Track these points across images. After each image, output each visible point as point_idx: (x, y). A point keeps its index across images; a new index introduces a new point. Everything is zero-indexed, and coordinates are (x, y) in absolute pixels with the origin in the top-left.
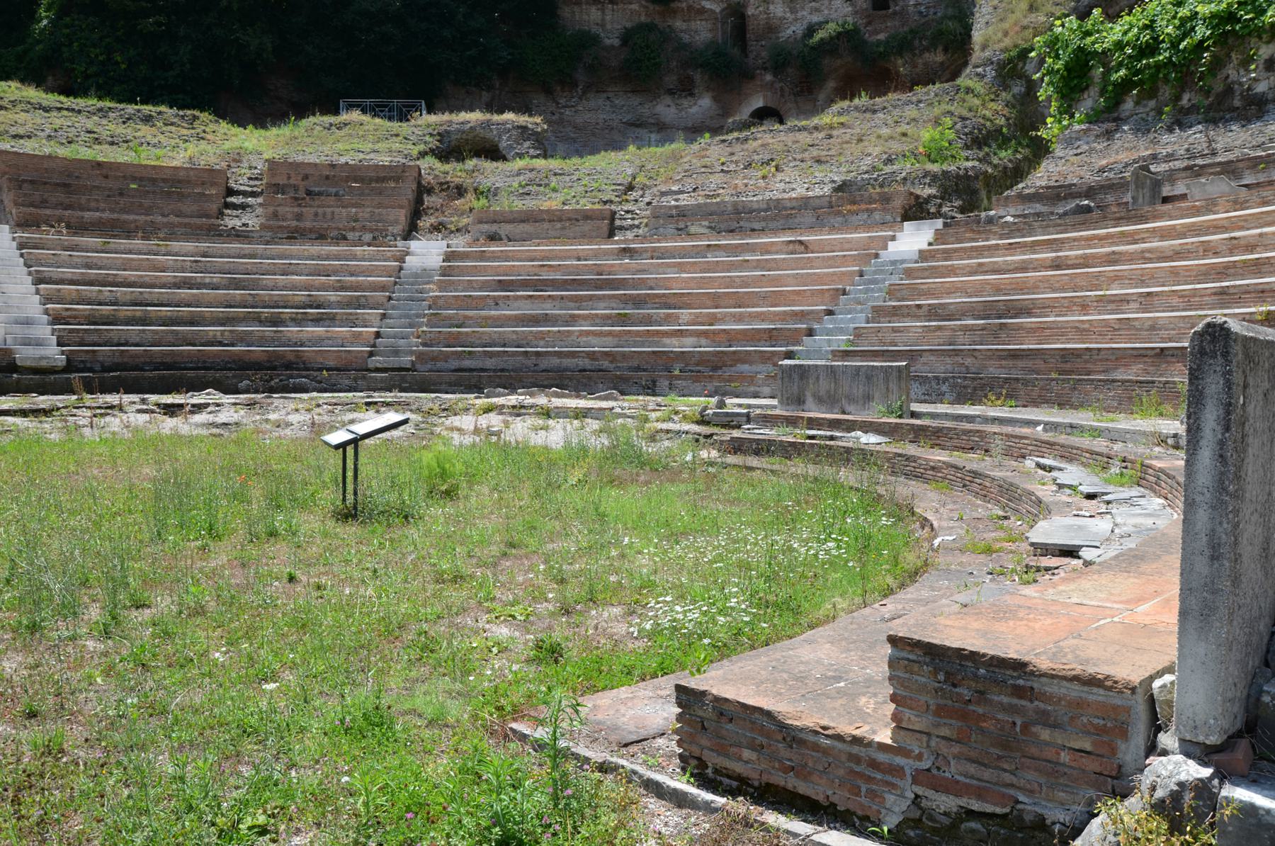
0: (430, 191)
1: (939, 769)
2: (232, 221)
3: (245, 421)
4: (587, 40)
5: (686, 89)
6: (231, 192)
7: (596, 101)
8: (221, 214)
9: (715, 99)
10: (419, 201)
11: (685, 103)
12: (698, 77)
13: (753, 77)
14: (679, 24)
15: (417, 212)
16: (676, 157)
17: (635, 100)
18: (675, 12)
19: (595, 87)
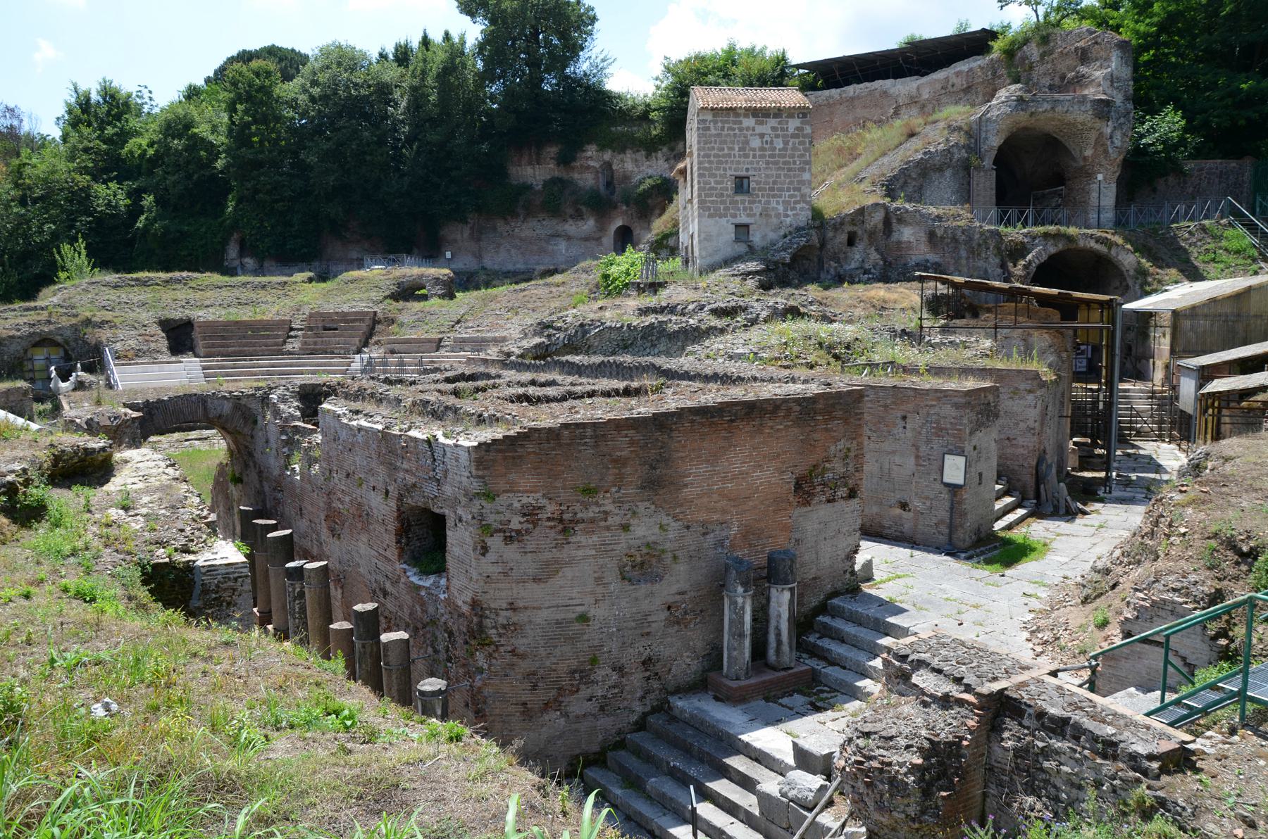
0: (379, 322)
1: (675, 558)
2: (289, 347)
3: (727, 286)
4: (527, 188)
5: (578, 216)
6: (292, 329)
7: (533, 223)
8: (285, 342)
9: (596, 221)
10: (373, 328)
11: (580, 223)
12: (584, 209)
13: (615, 207)
14: (576, 176)
15: (370, 334)
16: (494, 299)
17: (554, 222)
18: (573, 168)
19: (530, 213)
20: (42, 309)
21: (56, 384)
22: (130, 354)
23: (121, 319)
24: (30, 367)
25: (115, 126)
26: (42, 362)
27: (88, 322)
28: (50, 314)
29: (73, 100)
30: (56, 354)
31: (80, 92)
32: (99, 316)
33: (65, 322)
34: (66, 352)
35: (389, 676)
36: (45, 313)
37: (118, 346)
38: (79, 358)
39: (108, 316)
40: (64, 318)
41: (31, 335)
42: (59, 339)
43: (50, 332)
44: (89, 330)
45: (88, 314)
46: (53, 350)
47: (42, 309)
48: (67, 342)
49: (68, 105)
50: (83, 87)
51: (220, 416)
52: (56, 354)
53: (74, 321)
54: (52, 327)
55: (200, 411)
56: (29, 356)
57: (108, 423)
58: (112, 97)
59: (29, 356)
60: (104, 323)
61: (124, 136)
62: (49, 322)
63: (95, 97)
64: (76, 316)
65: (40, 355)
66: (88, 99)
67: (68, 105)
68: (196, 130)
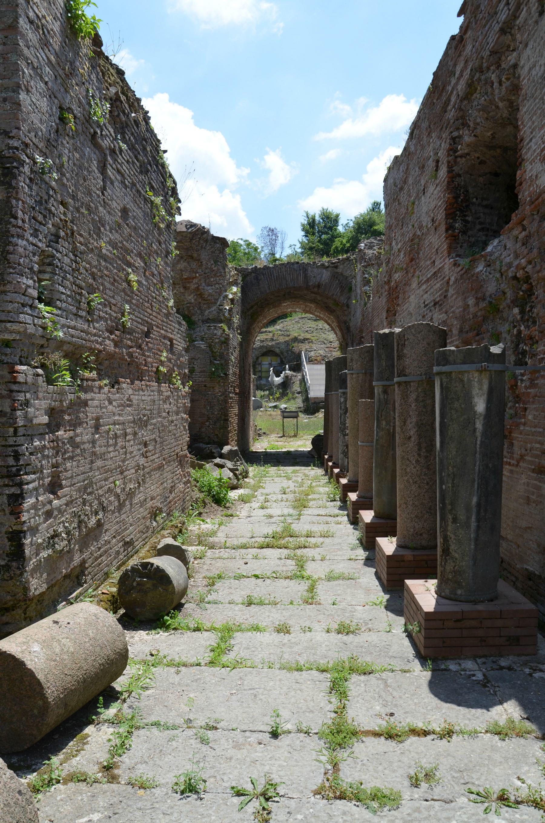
20: (270, 332)
21: (272, 378)
22: (318, 359)
23: (316, 338)
24: (260, 369)
25: (329, 234)
26: (267, 366)
27: (295, 339)
28: (274, 335)
29: (306, 222)
30: (276, 361)
31: (310, 216)
32: (302, 336)
33: (282, 339)
34: (281, 359)
35: (405, 397)
36: (271, 334)
37: (312, 354)
38: (288, 362)
39: (308, 336)
40: (281, 337)
41: (261, 347)
42: (277, 350)
43: (272, 346)
44: (296, 344)
45: (296, 335)
46: (274, 358)
47: (270, 332)
48: (282, 353)
49: (303, 225)
50: (311, 213)
51: (319, 286)
52: (276, 361)
53: (287, 339)
54: (274, 343)
55: (301, 278)
56: (260, 362)
57: (184, 229)
58: (328, 218)
59: (260, 362)
60: (305, 339)
61: (333, 238)
62: (272, 340)
63: (317, 218)
64: (289, 336)
65: (266, 361)
66: (314, 220)
67: (303, 225)
68: (375, 228)
